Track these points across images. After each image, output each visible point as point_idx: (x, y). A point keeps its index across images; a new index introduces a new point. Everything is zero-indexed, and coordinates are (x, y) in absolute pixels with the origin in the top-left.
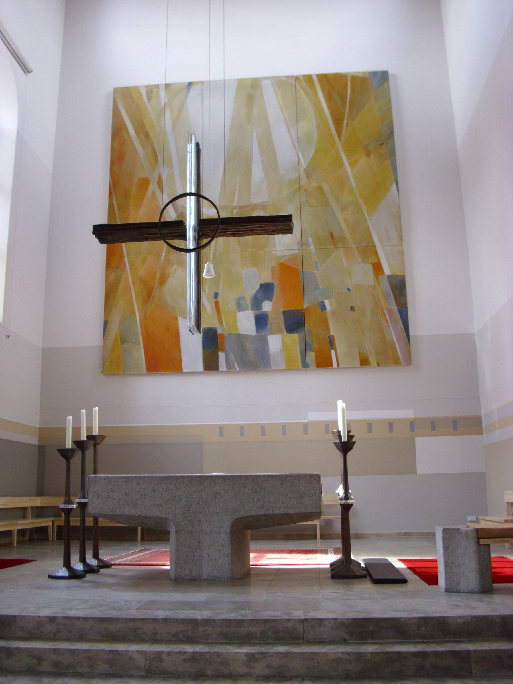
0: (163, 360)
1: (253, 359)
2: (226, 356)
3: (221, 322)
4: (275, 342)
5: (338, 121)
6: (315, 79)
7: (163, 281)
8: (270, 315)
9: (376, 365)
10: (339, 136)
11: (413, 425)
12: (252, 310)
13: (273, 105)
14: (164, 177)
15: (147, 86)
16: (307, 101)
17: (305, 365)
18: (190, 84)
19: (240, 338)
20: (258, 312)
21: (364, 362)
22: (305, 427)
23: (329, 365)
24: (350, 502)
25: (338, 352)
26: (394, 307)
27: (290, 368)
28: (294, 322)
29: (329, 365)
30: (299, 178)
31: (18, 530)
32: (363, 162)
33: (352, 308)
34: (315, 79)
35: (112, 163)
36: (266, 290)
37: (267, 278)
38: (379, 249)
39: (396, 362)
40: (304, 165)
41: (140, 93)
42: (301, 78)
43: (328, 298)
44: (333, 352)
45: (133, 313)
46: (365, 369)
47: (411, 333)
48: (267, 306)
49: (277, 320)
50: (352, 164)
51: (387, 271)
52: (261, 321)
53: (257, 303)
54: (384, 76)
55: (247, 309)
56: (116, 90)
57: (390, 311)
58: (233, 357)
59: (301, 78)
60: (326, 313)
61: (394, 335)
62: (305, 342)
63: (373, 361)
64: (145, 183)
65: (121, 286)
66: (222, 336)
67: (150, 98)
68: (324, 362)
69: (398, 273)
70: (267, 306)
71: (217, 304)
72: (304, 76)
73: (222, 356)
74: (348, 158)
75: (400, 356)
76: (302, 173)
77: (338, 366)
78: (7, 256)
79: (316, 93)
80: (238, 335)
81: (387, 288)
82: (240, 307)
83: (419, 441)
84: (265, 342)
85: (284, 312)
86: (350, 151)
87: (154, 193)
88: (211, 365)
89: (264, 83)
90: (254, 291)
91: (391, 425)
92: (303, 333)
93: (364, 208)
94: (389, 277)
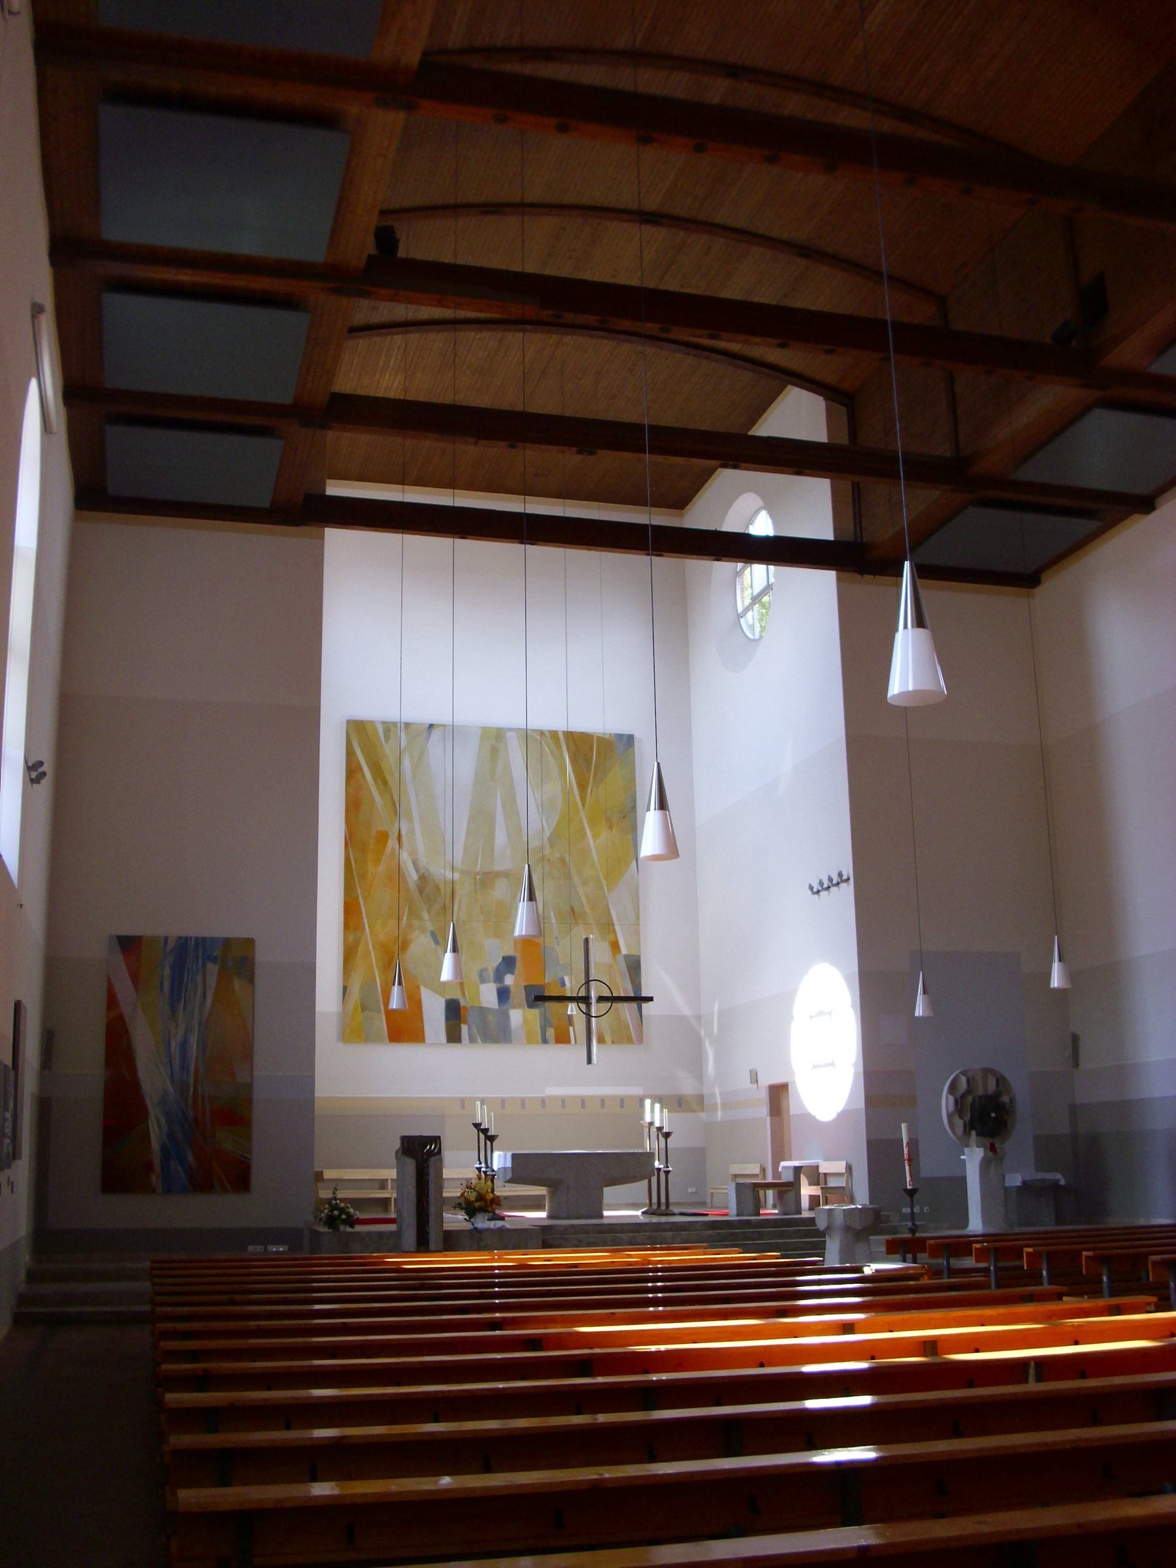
0: (405, 1028)
1: (496, 1032)
3: (463, 994)
4: (517, 1016)
5: (582, 787)
6: (561, 736)
7: (404, 946)
8: (512, 990)
10: (583, 805)
13: (515, 754)
14: (404, 832)
15: (384, 723)
16: (551, 760)
17: (545, 1041)
18: (431, 726)
19: (482, 1011)
20: (500, 985)
22: (543, 1101)
23: (568, 1042)
27: (530, 1040)
28: (538, 998)
29: (568, 1042)
30: (542, 847)
31: (1027, 1382)
32: (604, 835)
34: (561, 736)
35: (347, 810)
36: (508, 963)
37: (509, 951)
38: (618, 928)
39: (630, 1041)
40: (547, 833)
41: (376, 730)
45: (375, 980)
48: (509, 980)
49: (518, 994)
50: (595, 836)
51: (624, 951)
53: (499, 976)
54: (630, 739)
56: (349, 722)
58: (475, 1030)
62: (545, 1018)
63: (608, 1038)
64: (383, 837)
65: (361, 949)
66: (465, 1008)
67: (387, 738)
69: (634, 953)
70: (509, 980)
72: (550, 731)
73: (464, 1029)
74: (591, 830)
76: (546, 842)
78: (31, 654)
79: (562, 755)
80: (481, 1008)
81: (623, 964)
82: (483, 980)
84: (507, 1016)
85: (526, 987)
86: (593, 822)
87: (393, 849)
88: (454, 1037)
89: (509, 735)
90: (496, 964)
93: (604, 883)
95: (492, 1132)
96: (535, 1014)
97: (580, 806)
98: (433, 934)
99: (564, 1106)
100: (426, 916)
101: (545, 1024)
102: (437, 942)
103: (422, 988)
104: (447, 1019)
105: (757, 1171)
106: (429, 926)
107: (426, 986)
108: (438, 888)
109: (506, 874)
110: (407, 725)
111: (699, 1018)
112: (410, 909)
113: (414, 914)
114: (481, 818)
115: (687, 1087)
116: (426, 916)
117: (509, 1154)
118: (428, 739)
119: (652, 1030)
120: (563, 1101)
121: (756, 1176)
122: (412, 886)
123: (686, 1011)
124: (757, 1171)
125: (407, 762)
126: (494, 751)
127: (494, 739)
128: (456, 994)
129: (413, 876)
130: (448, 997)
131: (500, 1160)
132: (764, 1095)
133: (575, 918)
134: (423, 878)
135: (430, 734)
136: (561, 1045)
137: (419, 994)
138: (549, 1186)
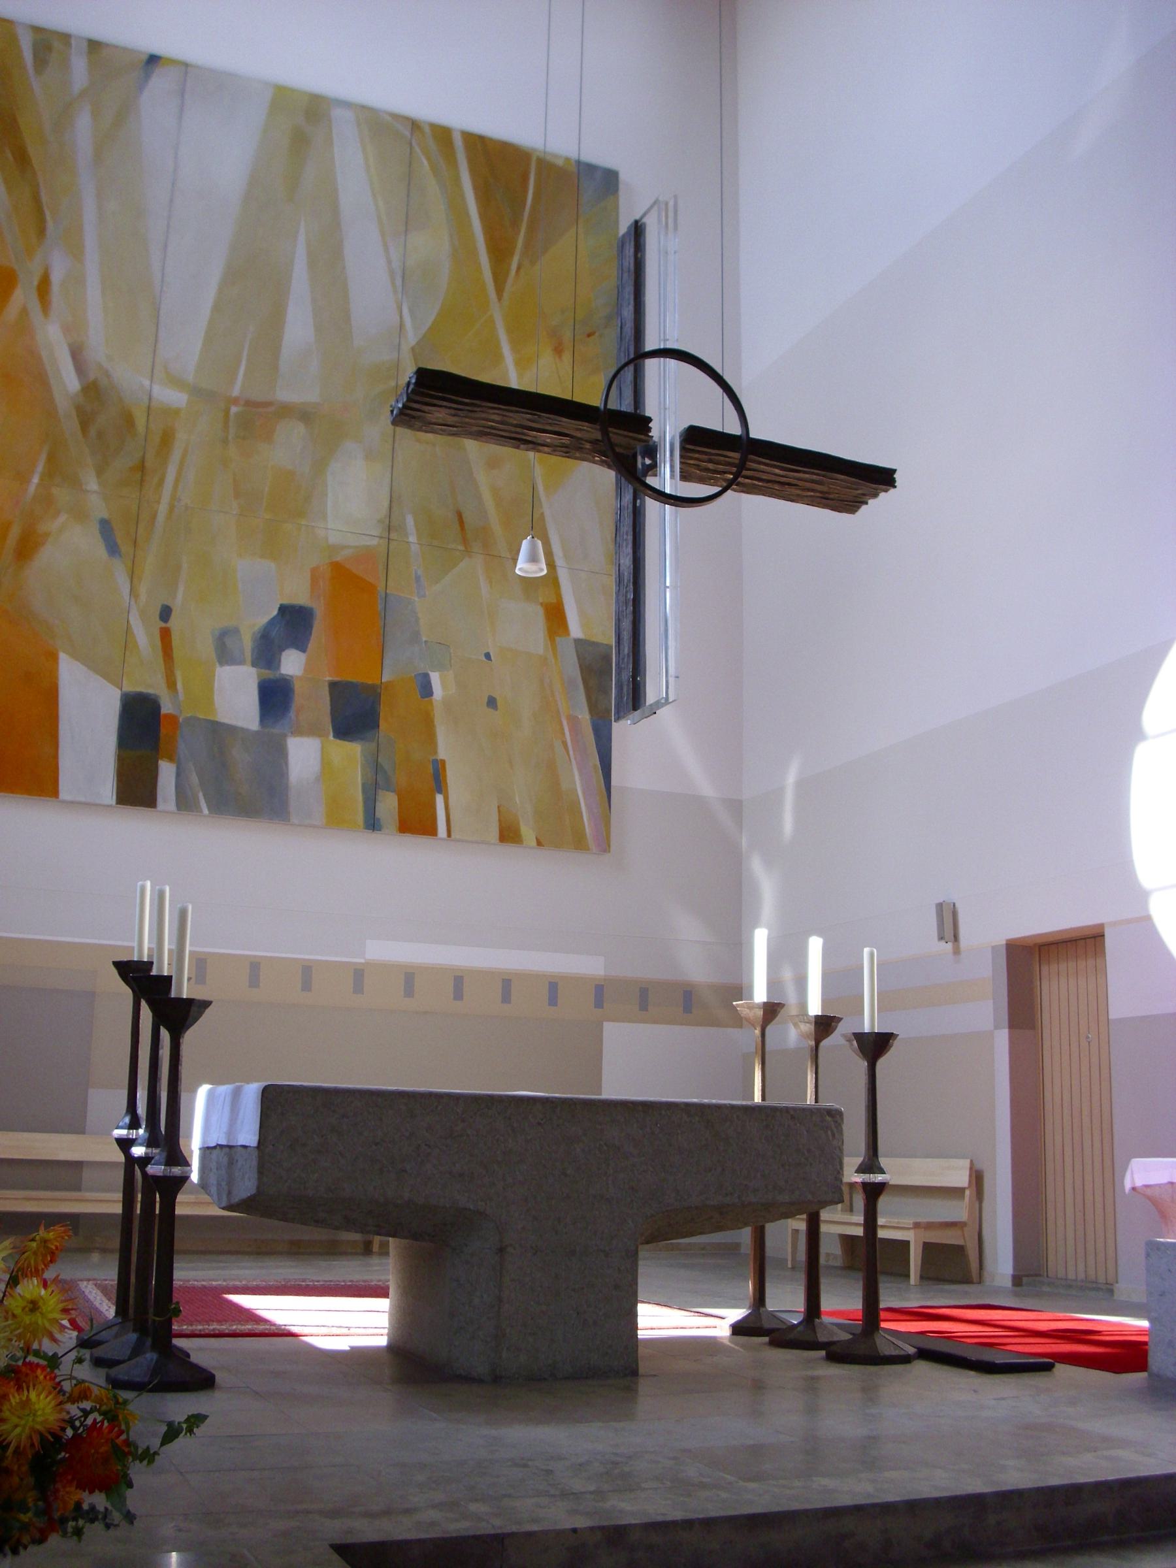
1: (249, 790)
2: (178, 775)
3: (171, 684)
4: (305, 755)
5: (500, 252)
6: (458, 142)
8: (298, 688)
9: (534, 843)
10: (500, 291)
11: (600, 991)
12: (253, 665)
14: (56, 277)
15: (37, 30)
17: (372, 824)
18: (153, 60)
19: (219, 733)
20: (268, 674)
21: (509, 834)
22: (359, 974)
24: (879, 1178)
25: (451, 800)
26: (584, 716)
27: (335, 820)
33: (492, 702)
34: (458, 142)
36: (293, 623)
37: (298, 593)
39: (579, 844)
41: (13, 40)
42: (427, 129)
43: (440, 667)
44: (439, 799)
46: (510, 849)
47: (615, 781)
48: (292, 663)
49: (312, 702)
52: (274, 697)
53: (267, 650)
55: (241, 662)
57: (574, 721)
58: (194, 779)
59: (427, 129)
60: (431, 703)
61: (577, 781)
63: (528, 833)
66: (173, 719)
68: (417, 822)
70: (292, 663)
71: (165, 634)
73: (167, 772)
74: (515, 348)
75: (587, 830)
77: (449, 835)
79: (457, 180)
80: (218, 723)
81: (572, 668)
82: (225, 655)
83: (608, 1027)
84: (280, 752)
85: (333, 685)
87: (24, 312)
88: (136, 789)
89: (337, 113)
90: (264, 620)
91: (554, 988)
92: (374, 745)
94: (578, 642)
95: (184, 990)
96: (351, 754)
97: (492, 295)
98: (106, 527)
99: (409, 991)
100: (92, 483)
101: (376, 781)
102: (113, 549)
103: (63, 658)
104: (124, 741)
105: (959, 1177)
106: (98, 507)
107: (75, 656)
108: (128, 420)
109: (305, 415)
110: (94, 46)
111: (736, 807)
112: (51, 458)
113: (58, 469)
114: (253, 284)
115: (696, 967)
116: (92, 483)
117: (252, 1091)
118: (141, 88)
119: (634, 825)
120: (410, 978)
121: (954, 1193)
122: (63, 405)
123: (706, 788)
124: (959, 1177)
125: (83, 126)
126: (300, 143)
127: (302, 119)
128: (151, 683)
129: (68, 381)
130: (130, 687)
131: (212, 1117)
132: (985, 971)
133: (465, 541)
134: (95, 392)
135: (147, 76)
136: (409, 839)
137: (51, 696)
138: (415, 1236)
